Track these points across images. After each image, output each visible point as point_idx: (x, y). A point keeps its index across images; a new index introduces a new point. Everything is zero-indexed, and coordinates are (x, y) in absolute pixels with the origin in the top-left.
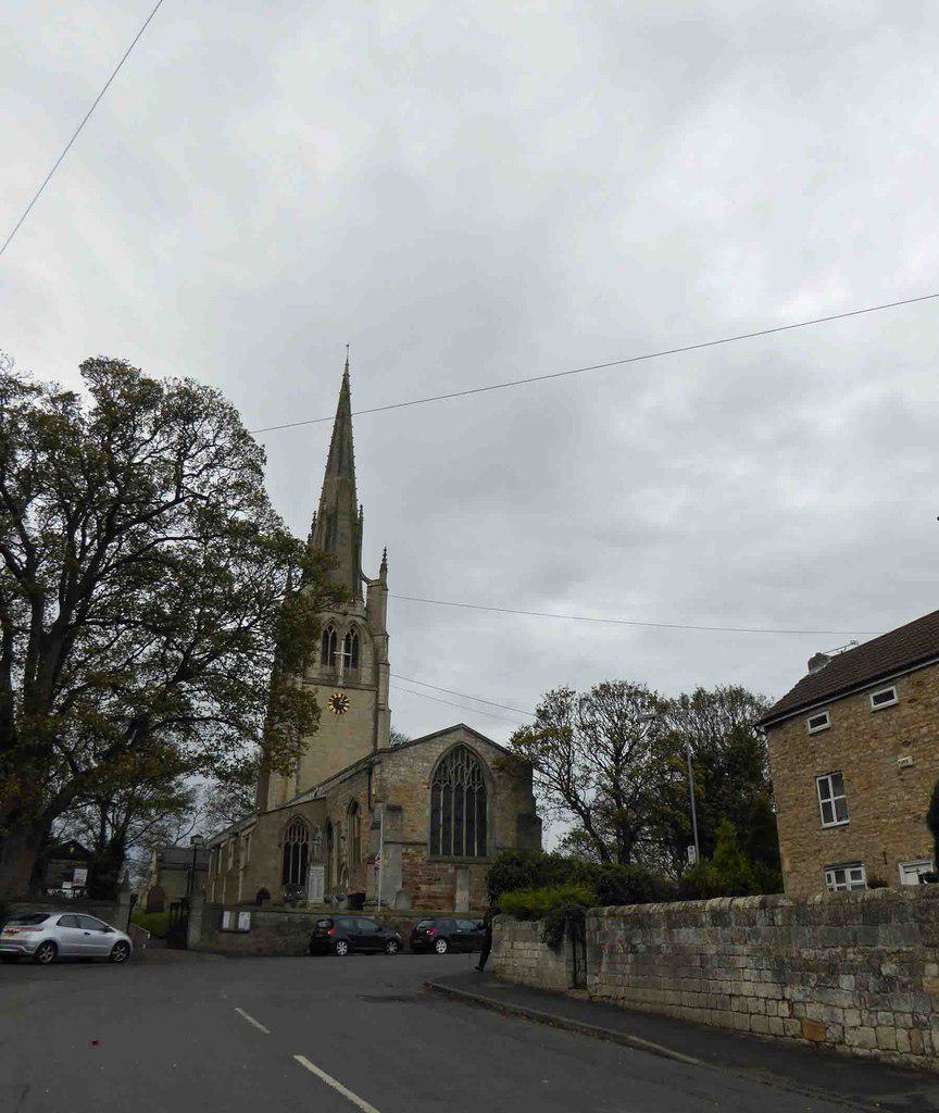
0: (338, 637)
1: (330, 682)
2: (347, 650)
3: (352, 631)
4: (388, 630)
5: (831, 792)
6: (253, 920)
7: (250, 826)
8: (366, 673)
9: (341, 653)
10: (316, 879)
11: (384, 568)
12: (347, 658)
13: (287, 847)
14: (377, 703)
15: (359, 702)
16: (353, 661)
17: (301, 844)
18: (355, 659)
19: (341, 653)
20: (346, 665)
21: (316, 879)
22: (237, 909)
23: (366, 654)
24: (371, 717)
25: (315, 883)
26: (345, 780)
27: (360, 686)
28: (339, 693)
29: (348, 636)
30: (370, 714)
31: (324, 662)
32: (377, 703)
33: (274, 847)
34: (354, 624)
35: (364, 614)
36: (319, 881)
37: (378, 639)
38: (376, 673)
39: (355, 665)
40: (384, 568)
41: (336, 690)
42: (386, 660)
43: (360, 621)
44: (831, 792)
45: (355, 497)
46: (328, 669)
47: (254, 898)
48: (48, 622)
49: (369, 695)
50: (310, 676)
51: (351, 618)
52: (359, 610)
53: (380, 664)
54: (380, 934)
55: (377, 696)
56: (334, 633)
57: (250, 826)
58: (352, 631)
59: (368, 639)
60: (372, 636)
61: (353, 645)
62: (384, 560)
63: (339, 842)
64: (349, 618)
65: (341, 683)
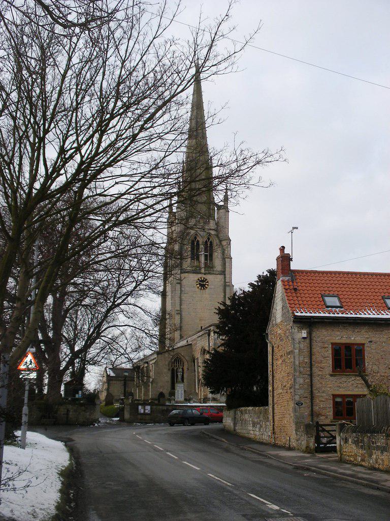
1: (196, 271)
2: (206, 250)
3: (209, 239)
4: (231, 236)
5: (333, 445)
6: (151, 409)
7: (153, 359)
8: (217, 263)
9: (202, 254)
12: (206, 256)
13: (173, 370)
14: (225, 282)
15: (214, 280)
16: (209, 257)
17: (175, 368)
18: (211, 255)
19: (202, 254)
20: (206, 259)
22: (144, 404)
23: (217, 255)
24: (222, 290)
26: (199, 337)
27: (214, 272)
30: (222, 288)
31: (192, 258)
32: (225, 282)
33: (165, 370)
34: (210, 234)
38: (224, 264)
39: (211, 260)
41: (200, 276)
43: (213, 232)
44: (333, 445)
46: (196, 263)
47: (157, 397)
48: (75, 351)
49: (221, 277)
52: (212, 225)
53: (226, 258)
54: (201, 416)
55: (225, 277)
57: (153, 359)
58: (209, 239)
60: (220, 241)
61: (209, 248)
63: (198, 370)
65: (203, 271)
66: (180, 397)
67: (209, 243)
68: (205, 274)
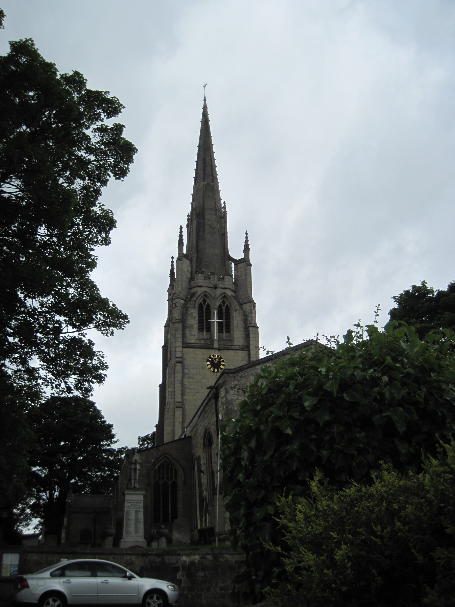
0: (212, 306)
2: (220, 317)
9: (215, 320)
10: (133, 512)
11: (247, 249)
12: (220, 324)
19: (215, 320)
20: (220, 330)
21: (133, 512)
25: (132, 516)
27: (233, 347)
28: (216, 354)
29: (220, 306)
31: (201, 329)
35: (233, 287)
36: (137, 512)
37: (247, 307)
39: (228, 331)
40: (247, 249)
41: (211, 352)
42: (255, 323)
43: (229, 293)
45: (219, 196)
46: (205, 335)
50: (188, 341)
51: (223, 291)
56: (208, 306)
59: (238, 307)
62: (247, 241)
64: (220, 291)
65: (216, 345)
66: (132, 529)
67: (224, 308)
68: (219, 349)
